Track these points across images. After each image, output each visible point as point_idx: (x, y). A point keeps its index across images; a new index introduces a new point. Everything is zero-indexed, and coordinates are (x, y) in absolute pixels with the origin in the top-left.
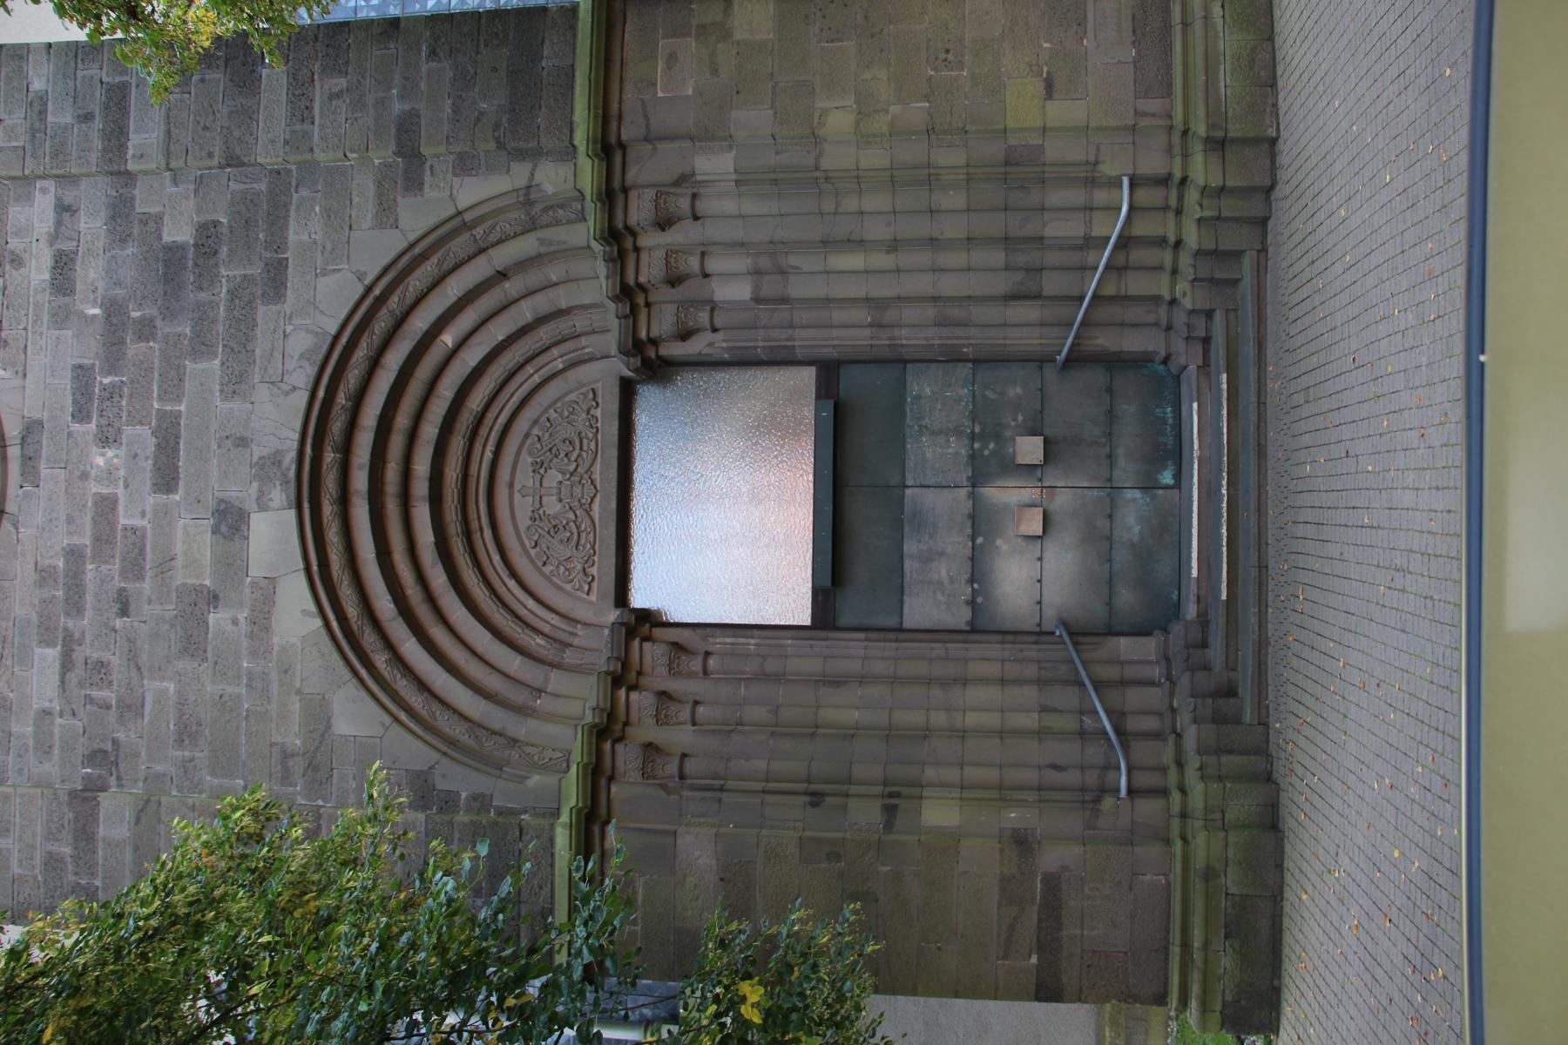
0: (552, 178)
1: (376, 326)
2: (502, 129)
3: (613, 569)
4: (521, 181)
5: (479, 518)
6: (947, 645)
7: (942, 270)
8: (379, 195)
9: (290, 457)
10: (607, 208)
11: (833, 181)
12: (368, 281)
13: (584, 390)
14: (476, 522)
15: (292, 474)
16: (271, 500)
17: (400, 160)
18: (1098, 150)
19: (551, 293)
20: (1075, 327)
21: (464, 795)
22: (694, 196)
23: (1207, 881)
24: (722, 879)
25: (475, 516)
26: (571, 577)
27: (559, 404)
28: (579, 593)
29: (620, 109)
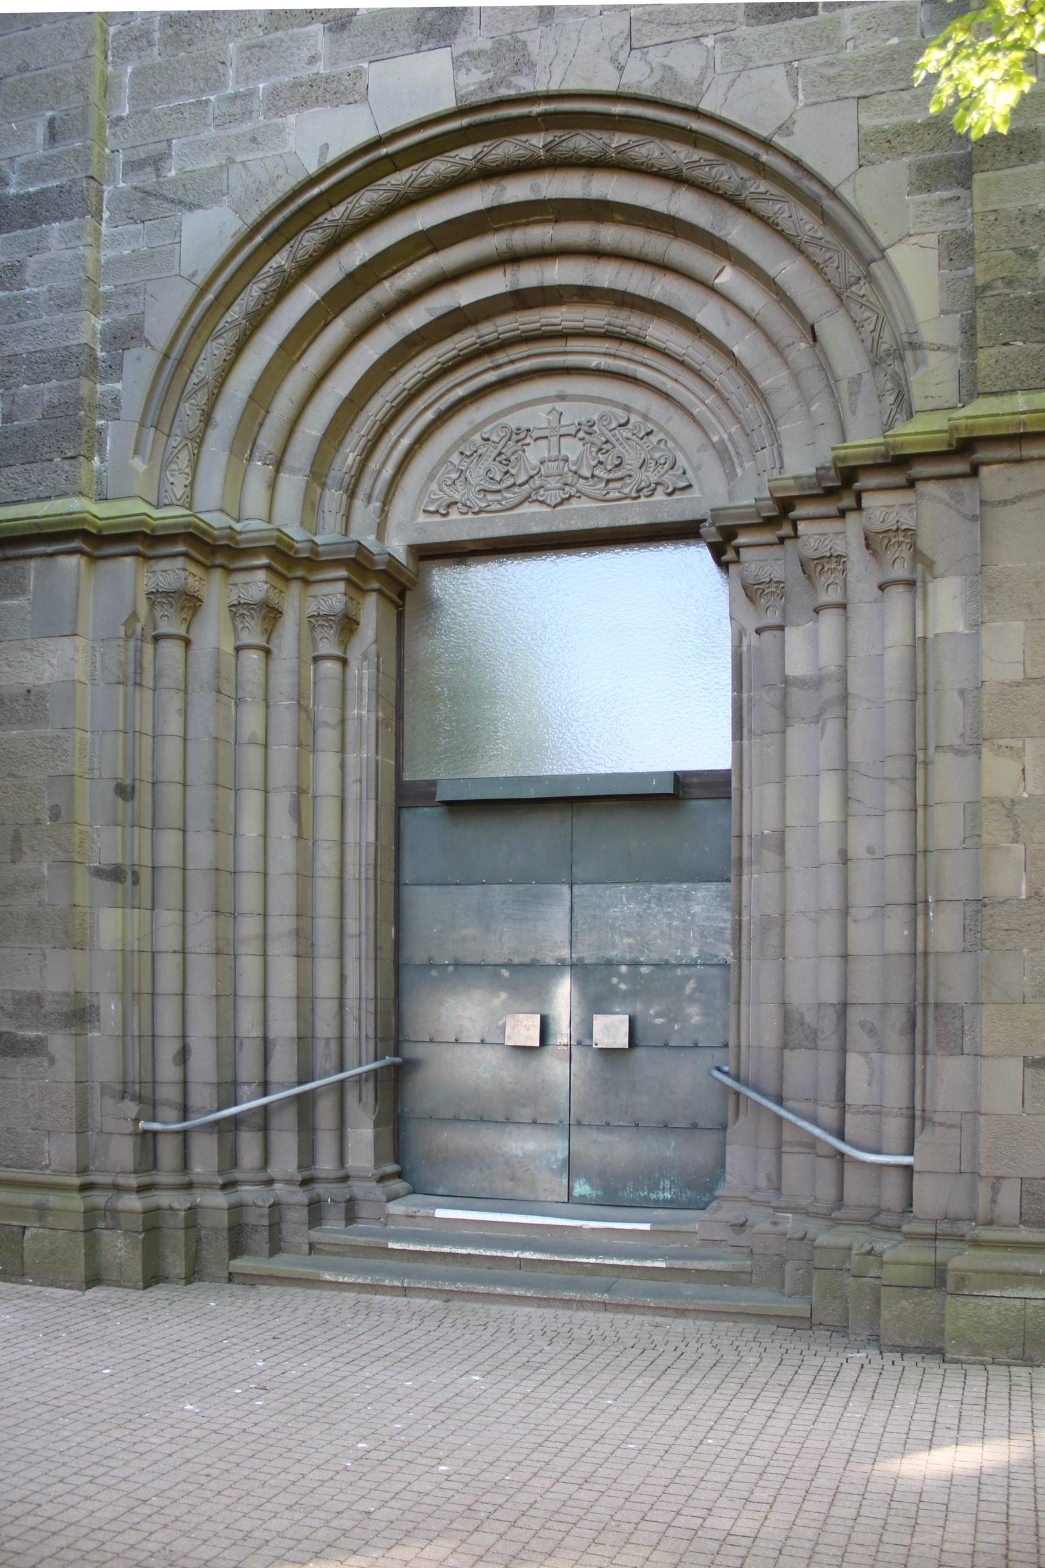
1: (722, 168)
2: (1007, 291)
3: (454, 539)
4: (928, 334)
5: (512, 362)
9: (526, 85)
10: (880, 461)
12: (779, 141)
13: (690, 474)
14: (507, 359)
15: (504, 92)
16: (469, 70)
18: (952, 1126)
21: (119, 386)
23: (34, 1207)
24: (29, 691)
25: (513, 357)
26: (445, 488)
27: (670, 444)
29: (1031, 459)
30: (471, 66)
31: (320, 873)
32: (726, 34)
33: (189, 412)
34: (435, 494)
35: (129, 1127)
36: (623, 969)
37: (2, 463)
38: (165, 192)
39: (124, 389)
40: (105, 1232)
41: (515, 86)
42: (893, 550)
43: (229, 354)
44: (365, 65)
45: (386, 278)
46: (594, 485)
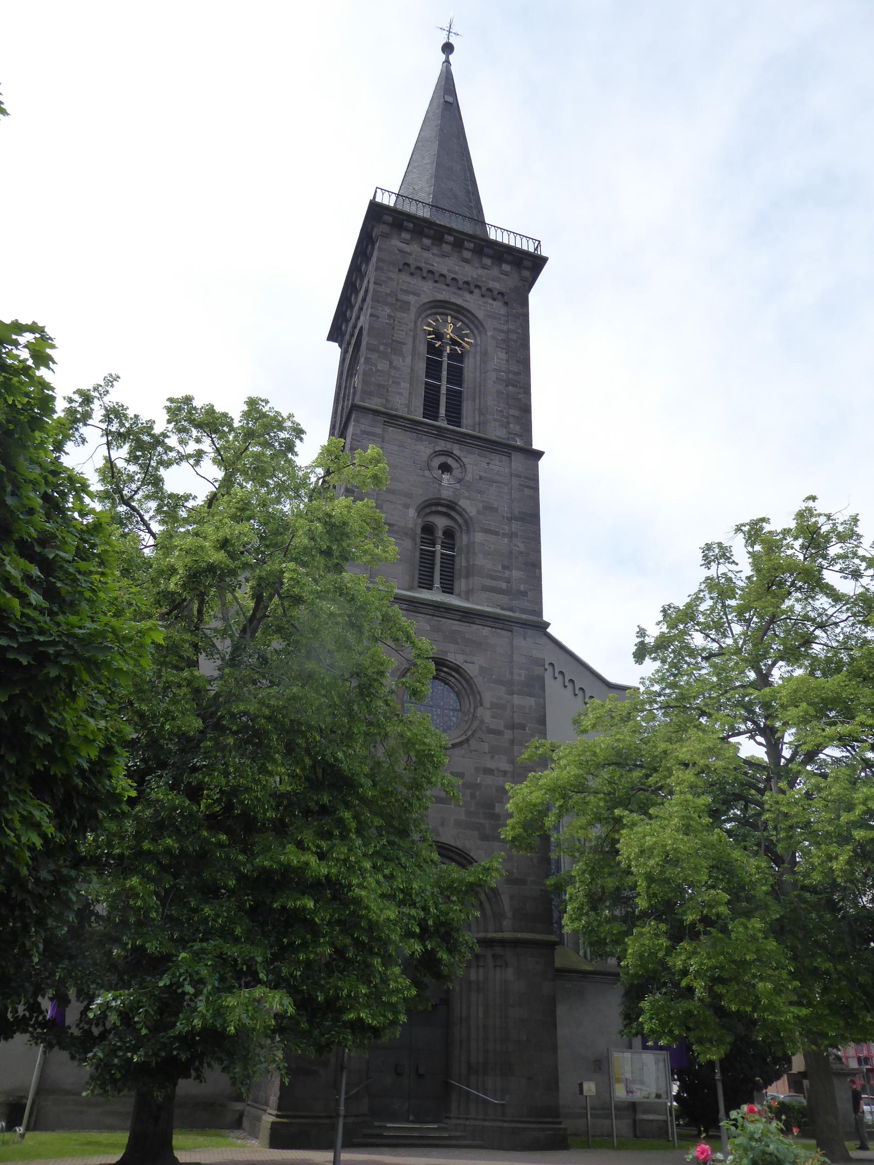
0: (507, 923)
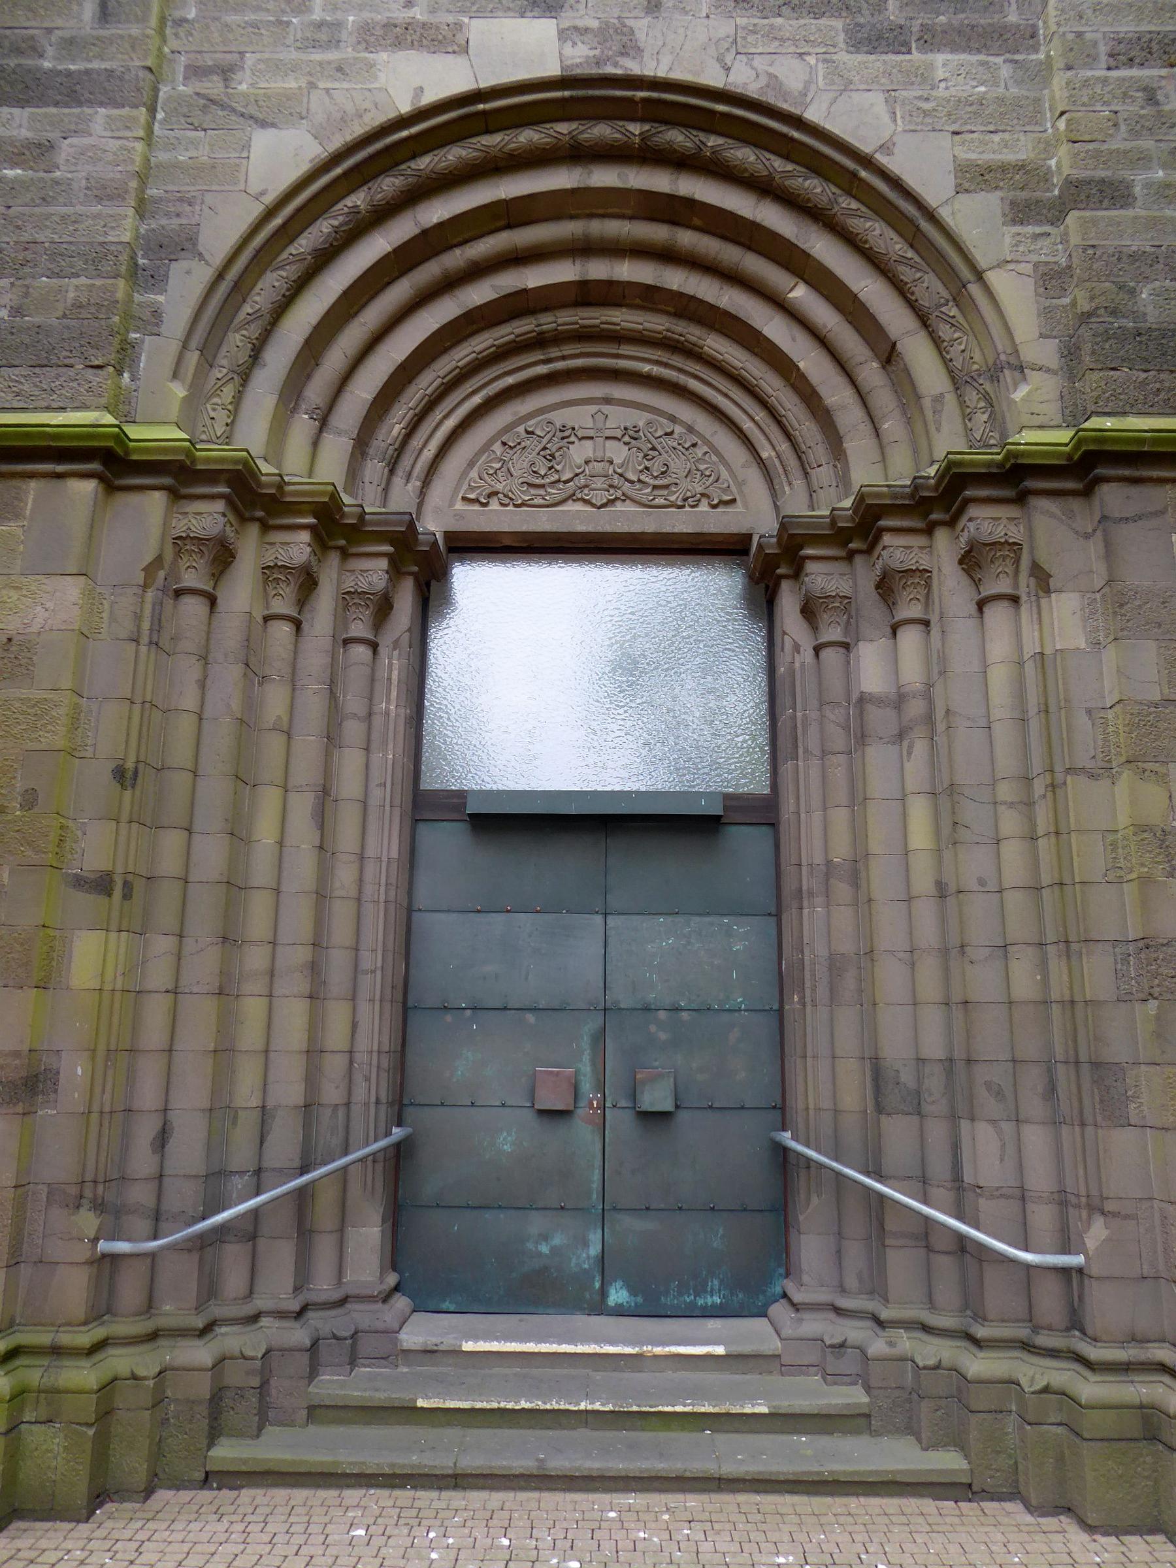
5: (564, 358)
6: (379, 973)
7: (913, 965)
8: (1004, 168)
9: (632, 67)
11: (1049, 795)
12: (882, 159)
13: (733, 488)
14: (559, 354)
15: (610, 70)
16: (574, 44)
17: (1056, 192)
18: (1127, 1217)
19: (865, 428)
20: (834, 1164)
21: (161, 298)
22: (1015, 600)
24: (10, 640)
27: (714, 458)
28: (465, 486)
30: (577, 40)
31: (337, 893)
32: (827, 56)
33: (240, 344)
34: (475, 482)
35: (82, 1252)
36: (662, 1015)
37: (4, 362)
38: (234, 105)
39: (167, 302)
40: (35, 1428)
41: (621, 67)
42: (997, 564)
43: (288, 290)
44: (466, 20)
45: (456, 246)
46: (640, 490)
